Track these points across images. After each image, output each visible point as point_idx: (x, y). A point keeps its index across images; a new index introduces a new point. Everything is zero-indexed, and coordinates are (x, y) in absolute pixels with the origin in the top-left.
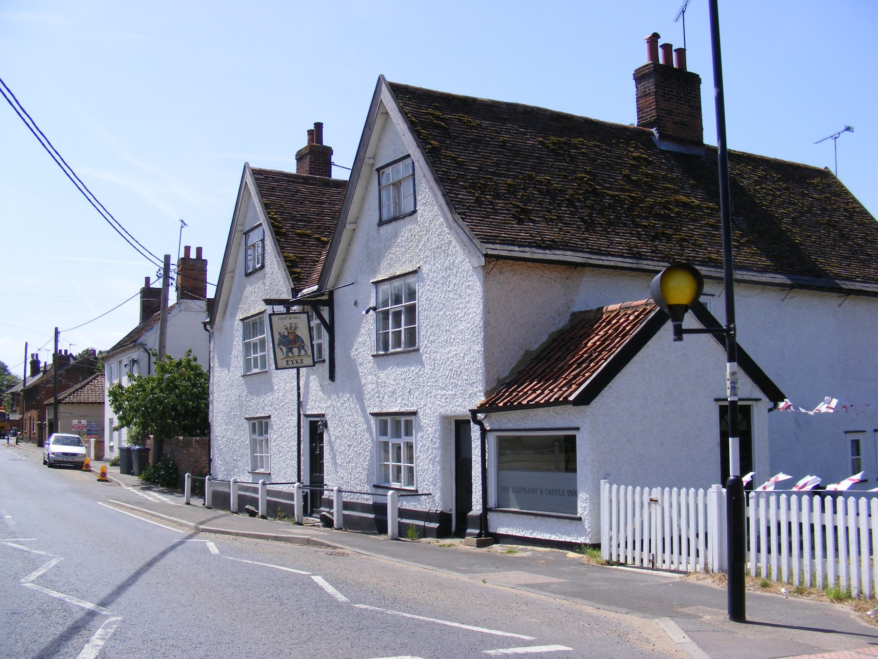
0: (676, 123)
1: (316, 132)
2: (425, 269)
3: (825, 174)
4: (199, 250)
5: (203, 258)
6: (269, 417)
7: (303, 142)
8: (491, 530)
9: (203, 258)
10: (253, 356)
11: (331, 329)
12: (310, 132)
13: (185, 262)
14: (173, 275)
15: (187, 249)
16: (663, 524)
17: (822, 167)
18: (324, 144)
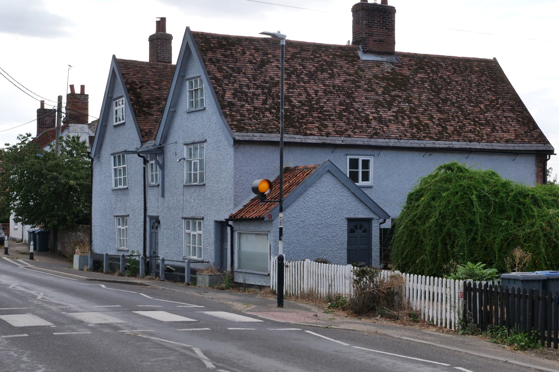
0: (376, 41)
1: (161, 24)
2: (209, 140)
4: (83, 87)
5: (86, 93)
6: (128, 216)
7: (153, 31)
8: (235, 281)
9: (86, 93)
10: (118, 177)
11: (162, 167)
13: (72, 97)
14: (64, 110)
15: (72, 87)
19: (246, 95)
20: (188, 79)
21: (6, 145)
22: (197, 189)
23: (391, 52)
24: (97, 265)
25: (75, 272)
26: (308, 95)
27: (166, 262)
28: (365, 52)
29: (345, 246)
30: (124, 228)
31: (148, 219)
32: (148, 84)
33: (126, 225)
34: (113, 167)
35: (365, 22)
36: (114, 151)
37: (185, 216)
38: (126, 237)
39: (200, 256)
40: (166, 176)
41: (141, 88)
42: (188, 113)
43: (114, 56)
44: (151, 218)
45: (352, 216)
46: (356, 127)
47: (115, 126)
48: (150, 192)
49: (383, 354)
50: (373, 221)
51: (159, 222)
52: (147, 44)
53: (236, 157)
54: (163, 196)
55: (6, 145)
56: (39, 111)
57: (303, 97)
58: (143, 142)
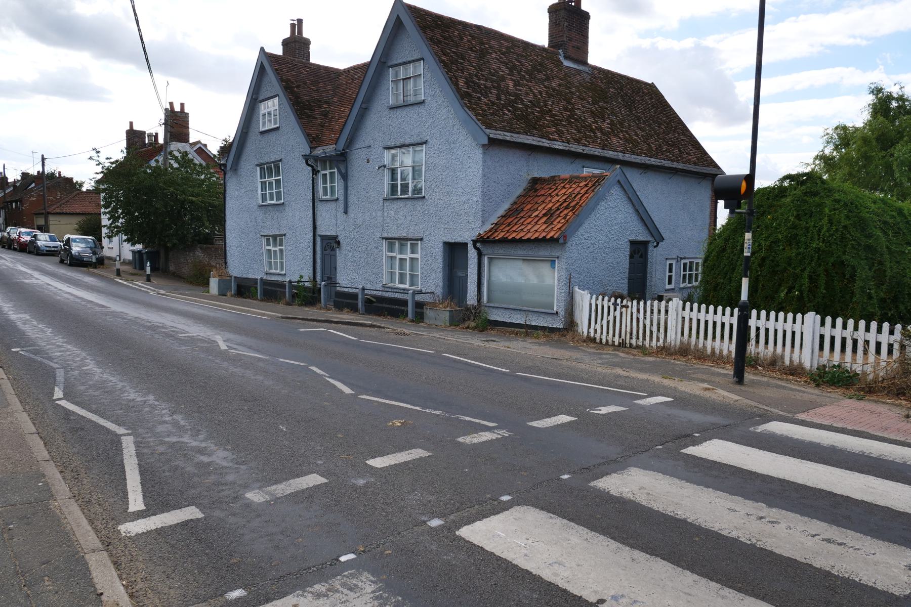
3: (652, 87)
4: (182, 105)
11: (345, 177)
12: (293, 26)
16: (683, 325)
17: (650, 82)
18: (313, 60)
19: (479, 87)
20: (392, 66)
21: (107, 159)
22: (409, 203)
23: (585, 63)
24: (244, 289)
25: (212, 298)
26: (535, 95)
27: (366, 292)
28: (566, 58)
29: (627, 275)
30: (277, 249)
31: (318, 239)
32: (305, 83)
33: (281, 245)
34: (259, 180)
35: (566, 24)
36: (261, 161)
37: (385, 235)
38: (282, 259)
39: (282, 269)
40: (350, 188)
41: (298, 87)
42: (391, 108)
43: (262, 49)
44: (323, 238)
45: (633, 238)
46: (586, 137)
47: (263, 133)
48: (320, 207)
49: (465, 356)
50: (650, 245)
51: (338, 243)
52: (125, 135)
53: (484, 161)
54: (346, 212)
55: (107, 159)
56: (128, 132)
57: (531, 97)
58: (312, 149)
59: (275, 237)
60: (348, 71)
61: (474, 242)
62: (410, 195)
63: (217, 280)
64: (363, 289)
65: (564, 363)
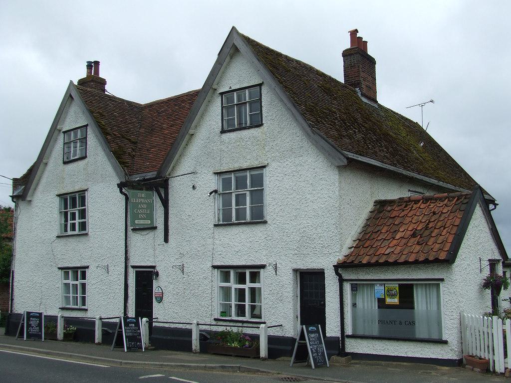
11: (165, 203)
51: (157, 274)
54: (166, 240)
59: (75, 269)
60: (151, 106)
61: (336, 267)
62: (248, 218)
63: (194, 347)
64: (101, 319)
65: (275, 372)
